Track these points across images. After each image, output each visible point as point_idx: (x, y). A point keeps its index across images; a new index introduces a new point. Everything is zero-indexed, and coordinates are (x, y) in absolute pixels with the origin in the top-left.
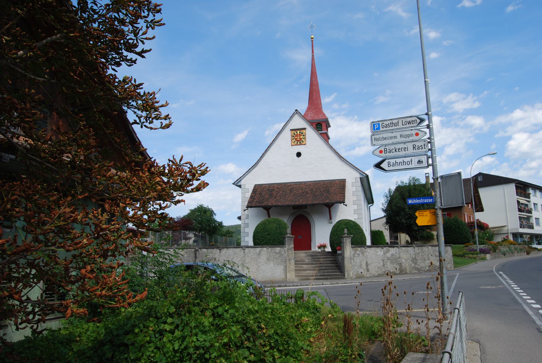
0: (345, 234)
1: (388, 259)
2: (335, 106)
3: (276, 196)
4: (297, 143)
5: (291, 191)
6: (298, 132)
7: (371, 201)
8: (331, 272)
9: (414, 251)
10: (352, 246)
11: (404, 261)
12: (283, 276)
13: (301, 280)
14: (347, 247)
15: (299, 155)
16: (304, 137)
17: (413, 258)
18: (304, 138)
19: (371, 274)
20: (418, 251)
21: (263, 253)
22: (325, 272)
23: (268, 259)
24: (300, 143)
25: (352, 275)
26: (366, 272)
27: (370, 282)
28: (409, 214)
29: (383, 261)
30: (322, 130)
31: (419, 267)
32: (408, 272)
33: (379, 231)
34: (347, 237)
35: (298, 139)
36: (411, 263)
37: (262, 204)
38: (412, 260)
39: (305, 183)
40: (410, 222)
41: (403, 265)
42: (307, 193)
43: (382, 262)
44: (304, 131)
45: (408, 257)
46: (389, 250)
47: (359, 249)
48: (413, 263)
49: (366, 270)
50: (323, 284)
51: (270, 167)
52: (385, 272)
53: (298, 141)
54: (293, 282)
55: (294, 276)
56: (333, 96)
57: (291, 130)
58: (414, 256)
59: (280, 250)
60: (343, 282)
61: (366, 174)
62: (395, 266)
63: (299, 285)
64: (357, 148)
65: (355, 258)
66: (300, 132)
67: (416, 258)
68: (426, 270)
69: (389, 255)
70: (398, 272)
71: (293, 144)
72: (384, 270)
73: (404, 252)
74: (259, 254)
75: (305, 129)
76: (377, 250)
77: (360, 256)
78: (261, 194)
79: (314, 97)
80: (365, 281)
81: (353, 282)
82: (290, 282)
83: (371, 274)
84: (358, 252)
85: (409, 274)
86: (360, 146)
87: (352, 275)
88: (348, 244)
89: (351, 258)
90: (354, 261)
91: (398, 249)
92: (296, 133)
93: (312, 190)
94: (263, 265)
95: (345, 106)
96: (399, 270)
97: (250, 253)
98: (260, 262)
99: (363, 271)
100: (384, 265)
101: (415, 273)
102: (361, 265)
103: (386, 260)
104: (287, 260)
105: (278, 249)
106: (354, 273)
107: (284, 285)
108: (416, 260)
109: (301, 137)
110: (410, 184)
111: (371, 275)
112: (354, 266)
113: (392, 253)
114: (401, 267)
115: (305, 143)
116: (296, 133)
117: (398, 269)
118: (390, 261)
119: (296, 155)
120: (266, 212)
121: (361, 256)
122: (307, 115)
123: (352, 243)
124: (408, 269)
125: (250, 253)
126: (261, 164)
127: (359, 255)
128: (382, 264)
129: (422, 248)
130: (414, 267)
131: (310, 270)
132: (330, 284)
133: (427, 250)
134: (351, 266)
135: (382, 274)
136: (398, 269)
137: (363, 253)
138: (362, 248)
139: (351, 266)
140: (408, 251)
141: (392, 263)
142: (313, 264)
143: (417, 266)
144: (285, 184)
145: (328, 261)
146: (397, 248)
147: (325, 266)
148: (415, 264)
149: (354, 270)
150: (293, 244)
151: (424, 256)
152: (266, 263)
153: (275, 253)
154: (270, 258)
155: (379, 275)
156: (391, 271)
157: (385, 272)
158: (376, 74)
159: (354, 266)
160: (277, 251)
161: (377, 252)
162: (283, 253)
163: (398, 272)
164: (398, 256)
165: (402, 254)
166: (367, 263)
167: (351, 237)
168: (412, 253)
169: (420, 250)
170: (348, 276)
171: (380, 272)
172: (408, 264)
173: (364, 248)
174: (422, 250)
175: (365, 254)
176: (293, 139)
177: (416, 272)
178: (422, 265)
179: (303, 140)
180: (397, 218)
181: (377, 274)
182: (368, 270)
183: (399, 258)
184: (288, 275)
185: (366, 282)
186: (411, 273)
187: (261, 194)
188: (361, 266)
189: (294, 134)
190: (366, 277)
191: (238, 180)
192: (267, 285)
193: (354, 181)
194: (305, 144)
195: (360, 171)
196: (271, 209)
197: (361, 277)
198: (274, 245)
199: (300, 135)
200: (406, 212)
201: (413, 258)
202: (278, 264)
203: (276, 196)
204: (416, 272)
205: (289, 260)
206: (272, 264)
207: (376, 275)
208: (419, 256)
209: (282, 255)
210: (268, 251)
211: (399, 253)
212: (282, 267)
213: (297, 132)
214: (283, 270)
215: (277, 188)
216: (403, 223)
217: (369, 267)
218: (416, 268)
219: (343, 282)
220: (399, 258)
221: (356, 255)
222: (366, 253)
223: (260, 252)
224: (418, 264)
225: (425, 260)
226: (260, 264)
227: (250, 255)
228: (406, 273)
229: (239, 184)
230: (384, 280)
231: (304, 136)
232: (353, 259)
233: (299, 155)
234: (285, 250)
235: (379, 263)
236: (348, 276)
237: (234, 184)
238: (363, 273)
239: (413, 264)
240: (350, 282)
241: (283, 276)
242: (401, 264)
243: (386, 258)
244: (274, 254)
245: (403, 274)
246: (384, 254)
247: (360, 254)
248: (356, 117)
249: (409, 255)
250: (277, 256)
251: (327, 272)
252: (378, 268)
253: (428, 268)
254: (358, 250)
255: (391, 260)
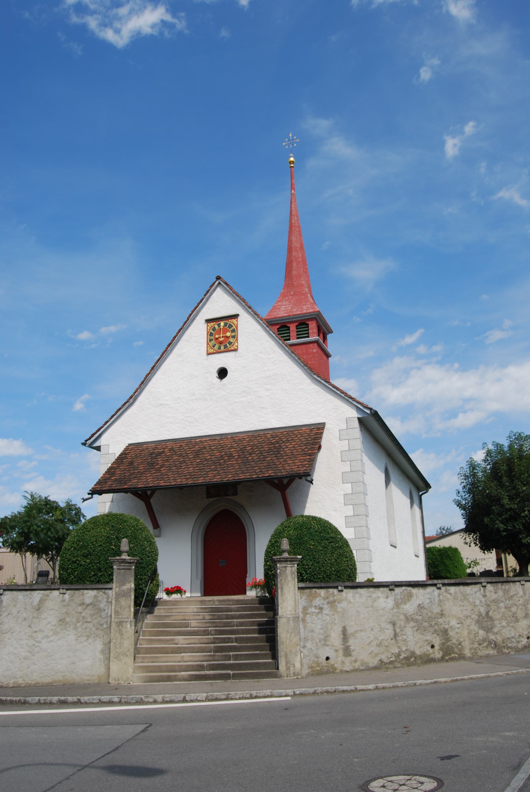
0: (284, 551)
1: (408, 619)
2: (422, 349)
3: (162, 466)
4: (219, 348)
5: (197, 454)
6: (222, 324)
7: (421, 484)
8: (247, 657)
9: (485, 596)
10: (302, 585)
11: (454, 623)
12: (101, 670)
13: (152, 680)
14: (286, 589)
15: (223, 373)
16: (233, 334)
17: (480, 615)
18: (234, 337)
19: (356, 661)
20: (494, 596)
21: (49, 604)
22: (229, 658)
23: (62, 621)
24: (225, 347)
25: (298, 665)
26: (341, 658)
27: (327, 692)
28: (511, 508)
29: (394, 624)
30: (308, 337)
31: (499, 639)
32: (467, 653)
33: (450, 548)
34: (286, 560)
35: (222, 339)
36: (474, 628)
37: (126, 483)
38: (478, 622)
39: (232, 437)
40: (514, 527)
41: (451, 633)
42: (231, 456)
43: (390, 627)
44: (234, 321)
45: (468, 613)
46: (410, 596)
47: (322, 592)
48: (482, 628)
49: (341, 652)
50: (184, 700)
51: (161, 405)
52: (399, 655)
53: (221, 343)
54: (130, 689)
55: (131, 670)
56: (417, 335)
57: (208, 321)
58: (483, 610)
59: (95, 596)
60: (246, 693)
61: (371, 409)
62: (429, 637)
63: (116, 699)
64: (461, 416)
65: (308, 618)
66: (226, 324)
67: (491, 614)
68: (520, 646)
69: (410, 608)
70: (437, 654)
71: (211, 351)
72: (396, 651)
73: (455, 598)
74: (39, 608)
75: (236, 316)
76: (374, 595)
77: (325, 611)
78: (131, 463)
79: (294, 272)
80: (311, 690)
81: (276, 692)
82: (117, 688)
83: (356, 661)
84: (317, 602)
85: (470, 659)
86: (465, 412)
87: (298, 665)
88: (289, 578)
89: (296, 619)
90: (305, 627)
91: (437, 592)
92: (216, 327)
93: (243, 450)
94: (47, 637)
95: (437, 348)
96: (441, 649)
97: (15, 606)
98: (41, 631)
99: (331, 654)
100: (396, 635)
101: (488, 656)
102: (326, 638)
103: (403, 623)
104: (113, 624)
105: (89, 595)
106: (305, 661)
107: (75, 699)
108: (491, 619)
109: (228, 334)
110: (511, 447)
111: (357, 665)
112: (306, 639)
113: (419, 602)
114: (448, 640)
115: (235, 347)
116: (216, 327)
117: (437, 647)
118: (412, 624)
119: (216, 375)
120: (142, 504)
121: (327, 610)
122: (279, 309)
123: (301, 579)
124: (467, 645)
125: (15, 606)
126: (142, 398)
127: (321, 609)
128: (390, 632)
129: (506, 586)
130: (484, 640)
131: (193, 650)
132: (208, 699)
133: (521, 593)
134: (295, 639)
135: (391, 662)
136: (437, 647)
137: (332, 604)
138: (331, 590)
139: (295, 639)
140: (465, 597)
141: (420, 628)
142: (206, 633)
143: (492, 637)
144: (189, 441)
145: (252, 624)
146: (435, 588)
147: (236, 640)
148: (488, 630)
149: (305, 651)
150: (133, 579)
151: (514, 609)
152: (56, 633)
153: (83, 604)
154: (68, 619)
155: (381, 666)
156: (418, 652)
157: (399, 655)
158: (485, 297)
159: (306, 639)
160: (88, 601)
161: (375, 601)
162: (102, 605)
163: (437, 654)
164: (436, 610)
165: (448, 606)
166: (344, 631)
167: (295, 560)
168: (477, 602)
169: (500, 593)
170: (288, 669)
171: (384, 657)
172: (465, 633)
173: (335, 591)
174: (505, 592)
175: (340, 606)
176: (211, 340)
177: (491, 652)
178: (508, 633)
179: (231, 340)
180: (486, 520)
181: (374, 662)
182: (347, 652)
183: (442, 614)
184: (114, 667)
185: (314, 693)
186: (475, 658)
187: (131, 463)
188: (325, 640)
189: (214, 329)
190: (342, 672)
191: (93, 435)
192: (29, 699)
193: (344, 426)
194: (236, 350)
195: (358, 402)
196: (155, 495)
197: (327, 672)
198: (99, 582)
199: (225, 331)
200: (503, 506)
201: (480, 615)
202: (88, 637)
203: (162, 466)
204: (491, 652)
205: (120, 624)
206: (71, 636)
207: (371, 665)
208: (499, 607)
209: (100, 610)
210: (63, 601)
211: (440, 601)
212: (99, 645)
213: (219, 325)
214: (102, 652)
215: (171, 449)
216: (498, 529)
217: (351, 642)
218: (490, 643)
219: (246, 693)
220: (442, 614)
221: (313, 610)
222: (344, 605)
223: (42, 601)
224: (495, 630)
225: (517, 620)
226: (40, 636)
227: (14, 611)
228: (462, 657)
229: (96, 445)
230: (371, 687)
231: (233, 331)
232: (304, 620)
233: (223, 373)
234: (108, 597)
235: (382, 630)
236: (288, 669)
237: (84, 444)
238: (331, 661)
239: (482, 633)
240: (268, 692)
241: (101, 670)
242: (445, 632)
243: (402, 617)
244: (80, 609)
245: (452, 659)
246: (397, 605)
247: (326, 606)
248: (456, 365)
249: (470, 608)
250: (87, 613)
251: (236, 657)
252: (379, 645)
253: (524, 641)
254: (320, 594)
255: (417, 621)
